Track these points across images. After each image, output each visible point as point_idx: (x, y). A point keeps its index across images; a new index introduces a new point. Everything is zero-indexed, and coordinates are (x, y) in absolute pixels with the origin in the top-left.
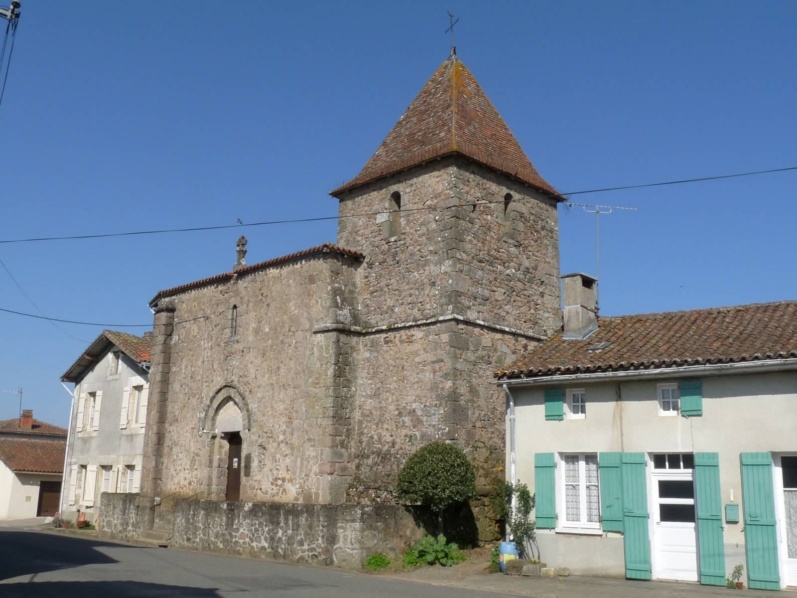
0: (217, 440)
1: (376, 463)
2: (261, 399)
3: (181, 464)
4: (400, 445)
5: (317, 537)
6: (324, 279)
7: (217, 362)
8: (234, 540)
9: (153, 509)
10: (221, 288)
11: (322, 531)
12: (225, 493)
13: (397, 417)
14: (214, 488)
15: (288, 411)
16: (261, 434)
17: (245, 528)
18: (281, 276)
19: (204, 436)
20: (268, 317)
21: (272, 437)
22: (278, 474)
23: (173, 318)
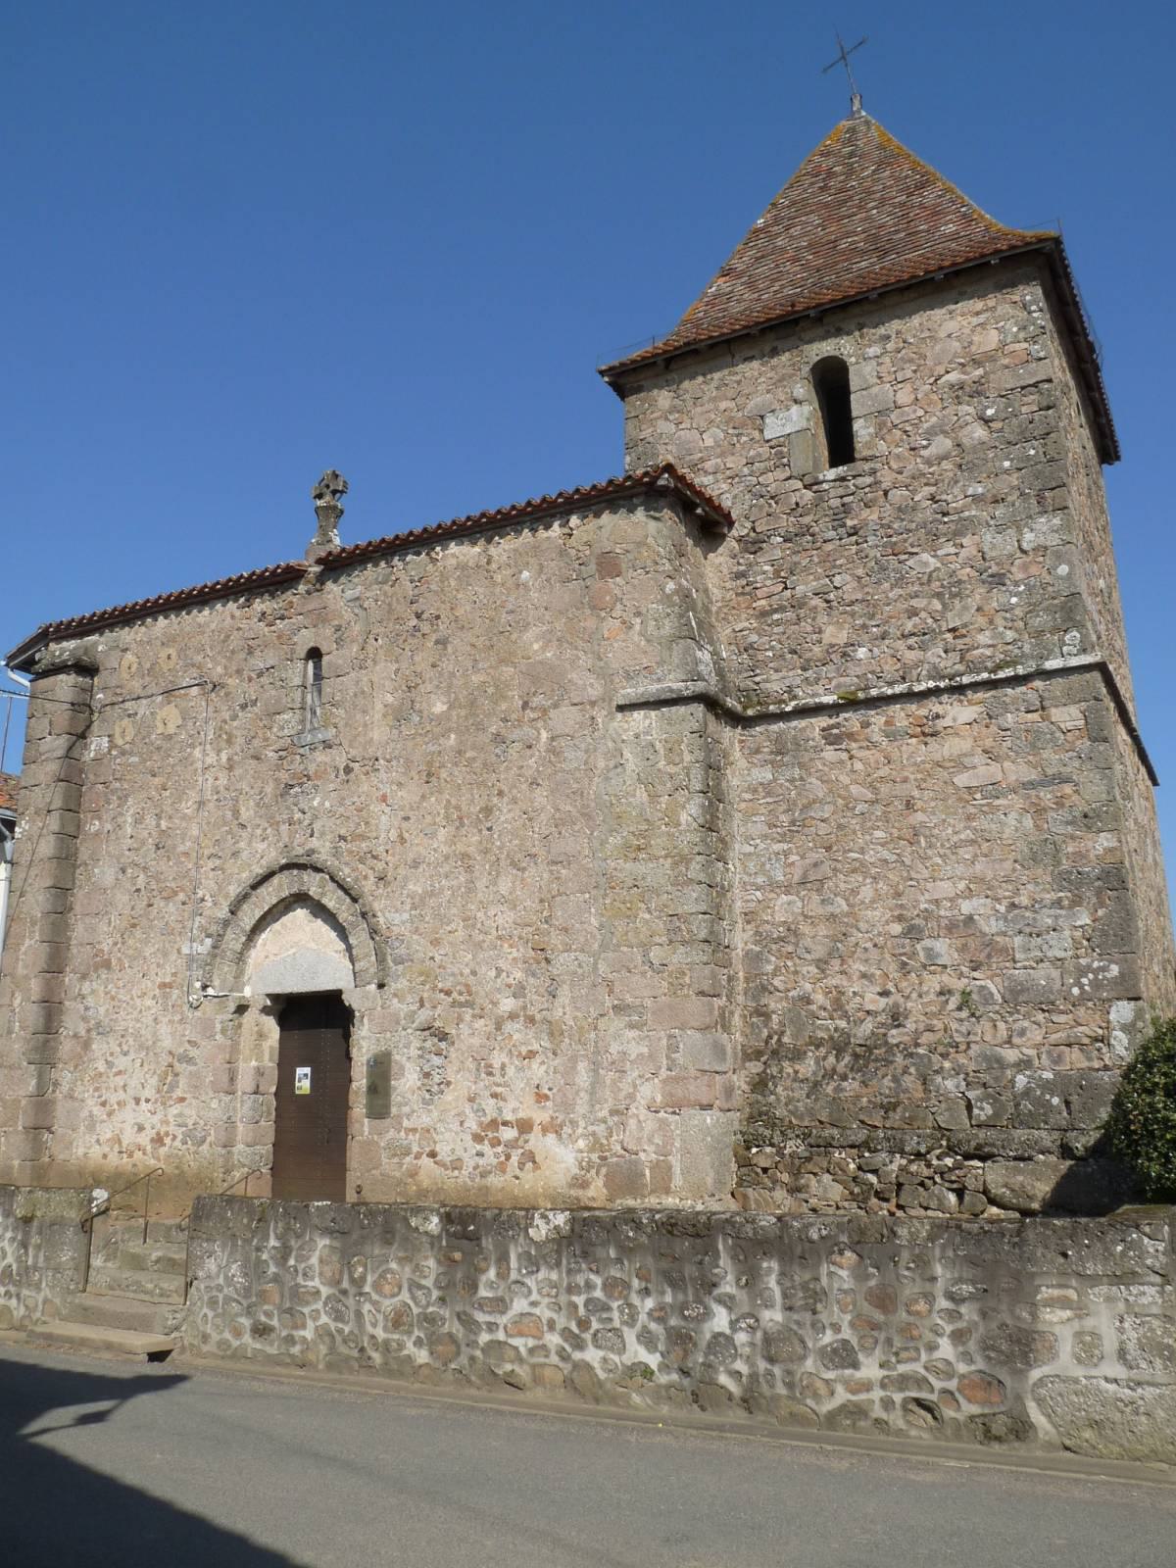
0: (251, 1017)
1: (834, 1070)
2: (422, 899)
3: (125, 1086)
4: (922, 1018)
5: (929, 1336)
6: (649, 563)
7: (252, 803)
8: (484, 1338)
9: (86, 1226)
10: (260, 605)
11: (953, 1315)
12: (269, 1166)
13: (900, 941)
14: (240, 1153)
15: (531, 929)
16: (425, 995)
17: (535, 1297)
18: (488, 563)
19: (208, 1007)
20: (441, 674)
21: (469, 1004)
22: (500, 1110)
23: (92, 691)
